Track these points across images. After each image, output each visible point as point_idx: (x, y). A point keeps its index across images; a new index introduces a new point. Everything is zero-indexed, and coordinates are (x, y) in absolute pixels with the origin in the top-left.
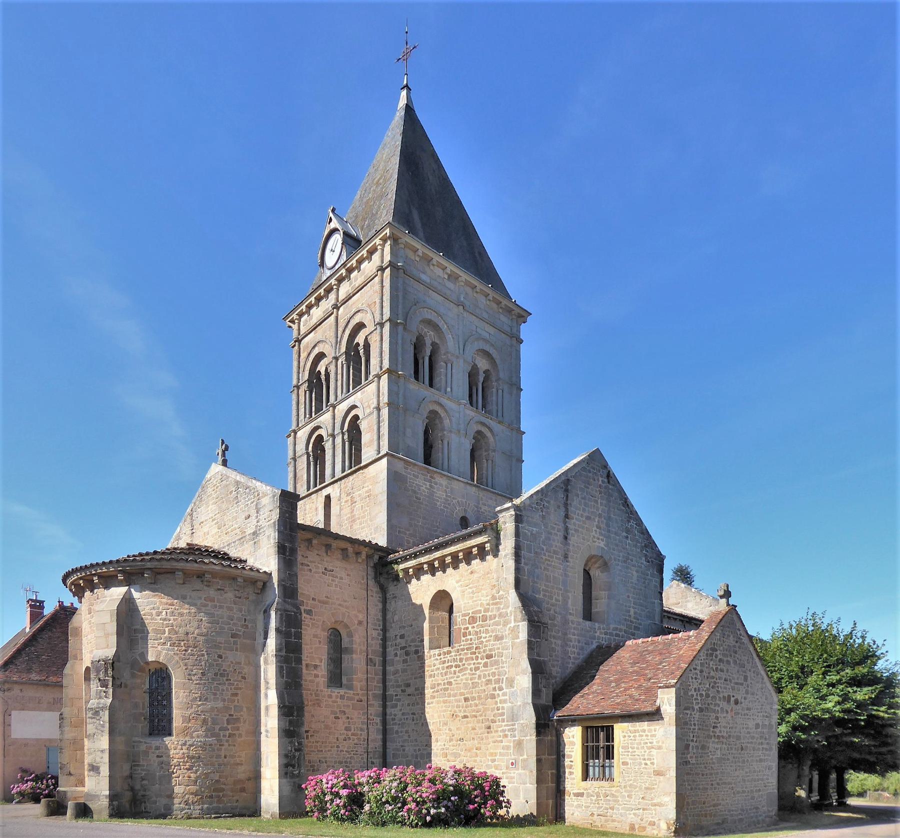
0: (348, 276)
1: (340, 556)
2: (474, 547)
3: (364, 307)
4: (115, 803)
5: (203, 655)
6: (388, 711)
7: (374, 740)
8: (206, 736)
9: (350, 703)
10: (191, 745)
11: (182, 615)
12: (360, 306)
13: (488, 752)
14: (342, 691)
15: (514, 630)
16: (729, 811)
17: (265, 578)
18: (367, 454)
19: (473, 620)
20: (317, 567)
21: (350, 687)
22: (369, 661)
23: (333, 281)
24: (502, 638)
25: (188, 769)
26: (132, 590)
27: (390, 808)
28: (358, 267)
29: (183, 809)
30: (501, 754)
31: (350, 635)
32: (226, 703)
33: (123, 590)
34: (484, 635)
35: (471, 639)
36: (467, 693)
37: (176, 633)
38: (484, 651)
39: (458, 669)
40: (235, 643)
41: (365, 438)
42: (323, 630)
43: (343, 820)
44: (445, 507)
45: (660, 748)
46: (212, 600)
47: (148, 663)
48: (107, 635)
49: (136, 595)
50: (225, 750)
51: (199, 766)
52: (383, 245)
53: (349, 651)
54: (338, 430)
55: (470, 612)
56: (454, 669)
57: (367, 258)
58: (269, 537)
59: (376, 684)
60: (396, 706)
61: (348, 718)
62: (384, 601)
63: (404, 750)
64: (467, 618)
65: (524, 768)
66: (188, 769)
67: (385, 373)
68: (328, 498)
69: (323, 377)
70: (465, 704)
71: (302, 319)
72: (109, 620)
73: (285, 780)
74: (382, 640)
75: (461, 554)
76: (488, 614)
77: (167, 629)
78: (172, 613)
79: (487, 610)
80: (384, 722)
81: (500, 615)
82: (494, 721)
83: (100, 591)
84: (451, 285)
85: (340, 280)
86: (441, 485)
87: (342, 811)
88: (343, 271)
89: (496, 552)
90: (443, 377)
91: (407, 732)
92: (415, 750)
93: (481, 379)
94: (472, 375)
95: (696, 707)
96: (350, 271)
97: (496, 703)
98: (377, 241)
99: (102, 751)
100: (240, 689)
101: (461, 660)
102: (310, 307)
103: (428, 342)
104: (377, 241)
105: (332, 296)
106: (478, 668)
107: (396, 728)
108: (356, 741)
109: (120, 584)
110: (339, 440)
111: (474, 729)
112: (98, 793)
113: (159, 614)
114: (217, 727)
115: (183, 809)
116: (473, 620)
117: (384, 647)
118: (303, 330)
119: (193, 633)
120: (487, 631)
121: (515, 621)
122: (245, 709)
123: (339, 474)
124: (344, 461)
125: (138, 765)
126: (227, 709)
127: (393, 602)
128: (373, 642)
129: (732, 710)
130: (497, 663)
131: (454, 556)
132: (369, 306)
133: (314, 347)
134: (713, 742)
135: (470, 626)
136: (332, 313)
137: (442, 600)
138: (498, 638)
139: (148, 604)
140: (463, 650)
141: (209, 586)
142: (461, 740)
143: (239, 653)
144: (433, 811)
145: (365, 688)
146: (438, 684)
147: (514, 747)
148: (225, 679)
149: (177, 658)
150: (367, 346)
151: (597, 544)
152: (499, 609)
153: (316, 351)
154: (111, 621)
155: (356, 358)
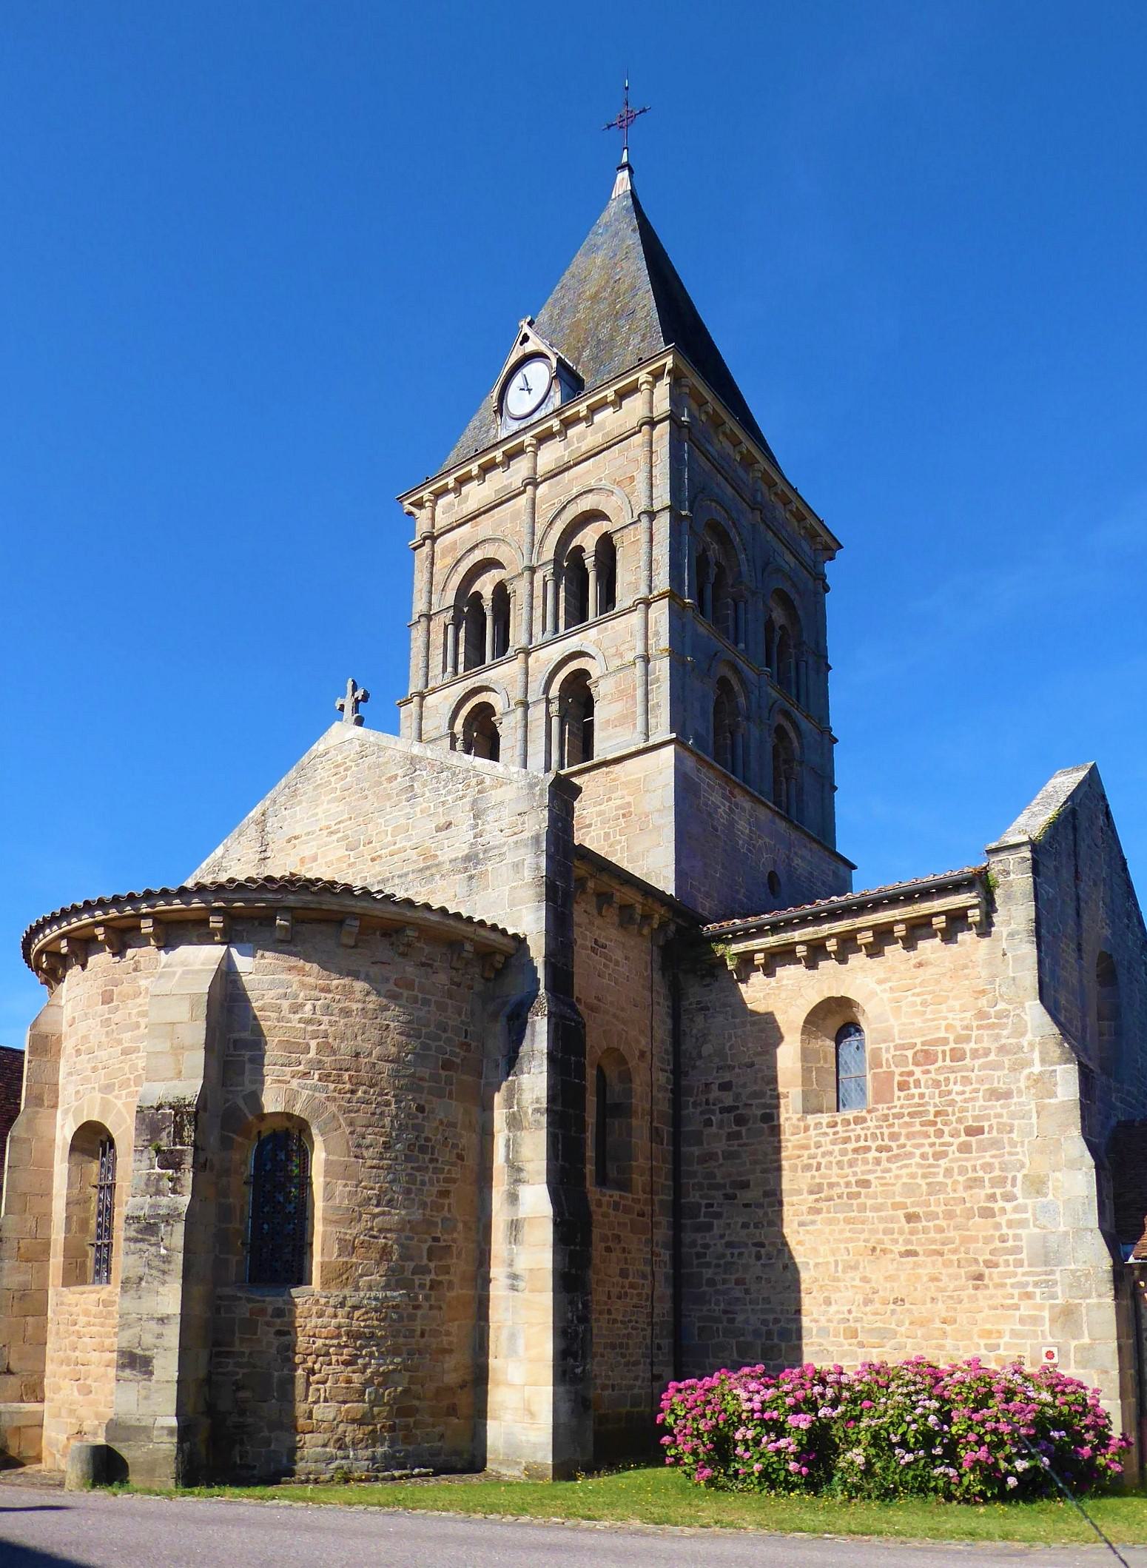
0: (563, 432)
1: (616, 919)
2: (897, 922)
4: (187, 1445)
5: (388, 1104)
6: (687, 1237)
8: (387, 1287)
10: (355, 1308)
11: (346, 1013)
12: (593, 483)
13: (976, 1329)
20: (585, 938)
22: (655, 1134)
23: (527, 439)
24: (1008, 1095)
25: (347, 1364)
26: (233, 951)
27: (909, 1457)
28: (588, 419)
29: (332, 1459)
30: (1014, 1334)
31: (626, 1077)
32: (428, 1212)
33: (217, 951)
34: (958, 1088)
35: (922, 1096)
36: (913, 1204)
37: (334, 1052)
38: (960, 1120)
39: (884, 1155)
40: (449, 1082)
43: (790, 1487)
44: (750, 851)
46: (409, 985)
47: (262, 1117)
48: (178, 1050)
49: (243, 963)
50: (424, 1317)
51: (371, 1355)
52: (653, 385)
54: (535, 693)
55: (918, 1041)
56: (873, 1154)
57: (613, 404)
58: (517, 866)
61: (624, 1250)
62: (676, 1015)
63: (732, 1321)
64: (910, 1053)
66: (347, 1364)
69: (487, 604)
70: (907, 1227)
71: (441, 502)
72: (185, 1016)
73: (562, 1389)
74: (672, 1091)
76: (968, 1047)
77: (313, 1044)
78: (327, 1010)
80: (677, 1261)
81: (1002, 1049)
82: (990, 1264)
83: (144, 955)
85: (543, 439)
86: (743, 809)
87: (792, 1466)
88: (555, 424)
89: (985, 928)
92: (765, 1322)
96: (568, 424)
97: (998, 1226)
98: (643, 376)
99: (162, 1320)
100: (454, 1181)
101: (894, 1137)
102: (462, 481)
104: (643, 376)
106: (945, 1154)
107: (708, 1273)
109: (207, 938)
110: (538, 713)
111: (934, 1279)
112: (147, 1422)
113: (296, 1009)
114: (410, 1265)
115: (332, 1459)
116: (926, 1057)
117: (677, 1104)
118: (442, 521)
119: (370, 1054)
120: (966, 1081)
121: (1043, 1061)
122: (460, 1226)
126: (430, 1223)
127: (699, 1019)
128: (660, 1095)
135: (918, 1071)
136: (524, 491)
137: (838, 1020)
139: (273, 985)
140: (900, 1116)
141: (403, 955)
143: (454, 1103)
144: (1021, 1465)
145: (648, 1189)
146: (831, 1185)
147: (1052, 1321)
148: (427, 1157)
149: (333, 1108)
152: (998, 1037)
154: (193, 1019)
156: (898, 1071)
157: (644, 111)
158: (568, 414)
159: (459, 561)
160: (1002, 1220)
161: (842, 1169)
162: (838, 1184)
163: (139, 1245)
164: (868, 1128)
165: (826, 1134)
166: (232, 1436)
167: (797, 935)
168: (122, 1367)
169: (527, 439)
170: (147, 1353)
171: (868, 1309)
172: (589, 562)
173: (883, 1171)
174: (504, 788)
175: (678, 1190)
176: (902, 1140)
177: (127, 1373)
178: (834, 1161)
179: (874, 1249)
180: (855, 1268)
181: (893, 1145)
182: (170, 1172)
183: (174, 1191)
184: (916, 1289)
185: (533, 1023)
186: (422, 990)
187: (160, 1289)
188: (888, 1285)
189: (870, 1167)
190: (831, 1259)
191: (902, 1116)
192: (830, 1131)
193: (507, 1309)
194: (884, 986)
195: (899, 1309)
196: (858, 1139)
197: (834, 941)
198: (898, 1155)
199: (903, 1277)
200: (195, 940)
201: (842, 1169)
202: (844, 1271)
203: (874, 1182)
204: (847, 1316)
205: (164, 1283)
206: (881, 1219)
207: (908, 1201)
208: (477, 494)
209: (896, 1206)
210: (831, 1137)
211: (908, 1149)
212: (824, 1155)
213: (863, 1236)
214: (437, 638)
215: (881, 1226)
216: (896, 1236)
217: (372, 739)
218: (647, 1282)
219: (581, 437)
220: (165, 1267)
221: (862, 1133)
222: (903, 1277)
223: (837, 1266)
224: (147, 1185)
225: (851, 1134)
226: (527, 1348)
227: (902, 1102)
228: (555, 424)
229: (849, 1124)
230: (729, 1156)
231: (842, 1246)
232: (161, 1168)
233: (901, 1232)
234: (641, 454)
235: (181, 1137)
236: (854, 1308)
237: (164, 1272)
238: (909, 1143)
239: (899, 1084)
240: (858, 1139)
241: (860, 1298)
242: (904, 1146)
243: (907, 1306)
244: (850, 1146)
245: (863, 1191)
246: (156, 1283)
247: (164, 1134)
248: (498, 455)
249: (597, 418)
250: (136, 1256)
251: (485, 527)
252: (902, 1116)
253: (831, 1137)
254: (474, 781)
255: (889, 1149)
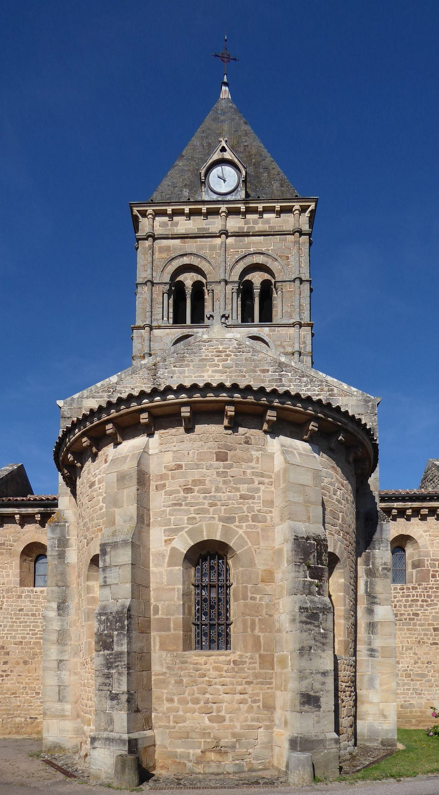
0: (244, 214)
23: (223, 208)
28: (261, 214)
39: (425, 603)
69: (189, 291)
88: (243, 208)
98: (297, 206)
99: (324, 674)
101: (429, 596)
102: (176, 213)
104: (297, 206)
140: (431, 588)
146: (401, 615)
156: (432, 569)
157: (235, 60)
158: (251, 205)
159: (173, 259)
161: (406, 608)
162: (404, 614)
163: (309, 626)
164: (418, 592)
165: (399, 593)
167: (395, 505)
168: (303, 704)
169: (223, 208)
170: (317, 694)
171: (416, 666)
172: (257, 291)
173: (424, 610)
174: (348, 397)
176: (433, 598)
177: (306, 707)
178: (403, 604)
179: (419, 642)
180: (411, 649)
181: (429, 600)
182: (316, 581)
183: (319, 594)
184: (436, 658)
185: (381, 525)
187: (322, 655)
188: (425, 656)
189: (418, 608)
190: (401, 645)
191: (433, 588)
192: (401, 591)
193: (368, 666)
194: (426, 534)
195: (429, 666)
196: (413, 596)
197: (410, 510)
198: (431, 604)
199: (431, 653)
200: (288, 434)
201: (406, 608)
202: (406, 650)
203: (421, 615)
204: (407, 668)
205: (324, 651)
206: (423, 630)
207: (435, 623)
208: (184, 225)
209: (429, 625)
210: (401, 594)
211: (435, 602)
212: (398, 601)
213: (414, 636)
215: (423, 632)
216: (429, 637)
217: (247, 343)
219: (255, 222)
220: (324, 641)
221: (415, 594)
222: (431, 653)
223: (403, 648)
224: (303, 588)
225: (411, 594)
226: (381, 685)
227: (433, 582)
228: (243, 208)
229: (410, 589)
231: (405, 640)
232: (311, 578)
233: (431, 635)
235: (321, 560)
236: (410, 666)
237: (324, 644)
238: (436, 600)
239: (432, 575)
240: (413, 596)
241: (413, 661)
242: (433, 600)
243: (432, 664)
244: (410, 599)
245: (416, 618)
246: (319, 651)
247: (311, 556)
248: (204, 208)
249: (265, 216)
250: (307, 634)
252: (433, 588)
253: (401, 594)
254: (326, 389)
255: (427, 601)
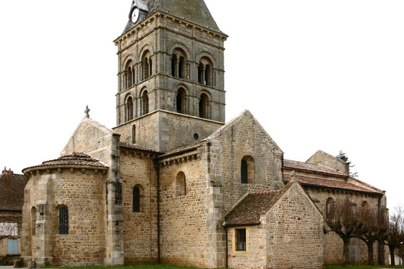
3: (149, 43)
6: (161, 222)
7: (154, 235)
9: (143, 219)
14: (139, 214)
15: (208, 190)
16: (295, 263)
17: (106, 169)
18: (151, 109)
19: (193, 185)
21: (143, 212)
22: (152, 201)
41: (150, 102)
42: (131, 188)
45: (261, 238)
46: (85, 179)
53: (143, 196)
59: (155, 209)
60: (163, 220)
64: (191, 184)
65: (212, 246)
67: (157, 75)
68: (134, 126)
69: (132, 70)
75: (193, 156)
79: (198, 181)
82: (201, 227)
84: (189, 30)
90: (186, 72)
91: (168, 231)
93: (204, 69)
94: (200, 67)
95: (277, 222)
103: (178, 57)
105: (135, 35)
107: (163, 229)
108: (146, 235)
109: (48, 173)
110: (139, 100)
116: (193, 185)
120: (198, 190)
123: (139, 116)
124: (141, 110)
125: (56, 247)
128: (154, 192)
129: (296, 222)
130: (202, 203)
131: (185, 158)
132: (151, 43)
133: (127, 57)
134: (286, 236)
138: (202, 193)
142: (189, 234)
150: (151, 61)
151: (248, 151)
153: (128, 58)
155: (146, 64)
160: (202, 218)
166: (370, 262)
175: (159, 212)
186: (88, 179)
214: (139, 67)
218: (150, 231)
230: (166, 205)
234: (154, 36)
251: (130, 49)
